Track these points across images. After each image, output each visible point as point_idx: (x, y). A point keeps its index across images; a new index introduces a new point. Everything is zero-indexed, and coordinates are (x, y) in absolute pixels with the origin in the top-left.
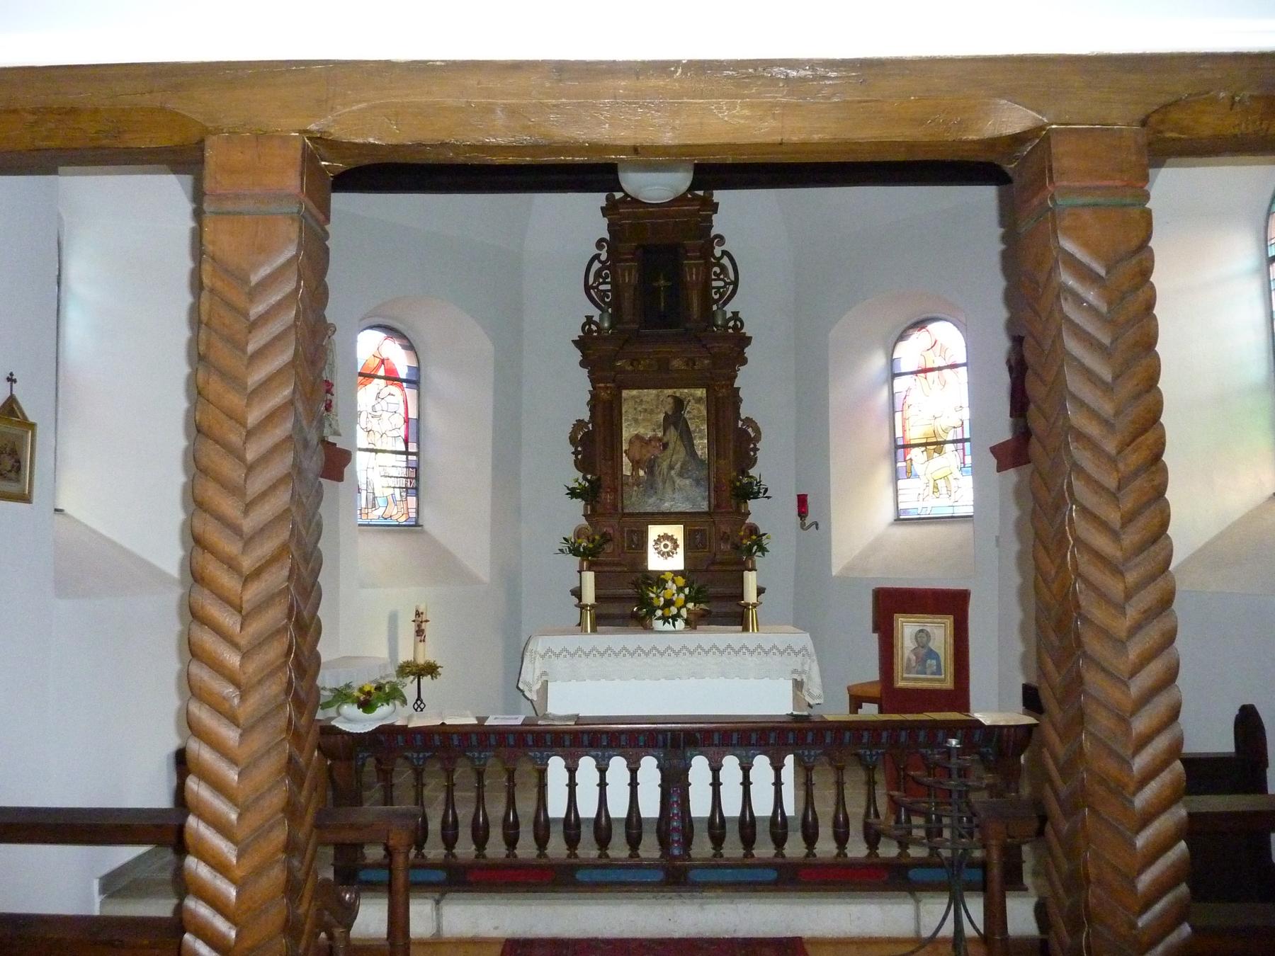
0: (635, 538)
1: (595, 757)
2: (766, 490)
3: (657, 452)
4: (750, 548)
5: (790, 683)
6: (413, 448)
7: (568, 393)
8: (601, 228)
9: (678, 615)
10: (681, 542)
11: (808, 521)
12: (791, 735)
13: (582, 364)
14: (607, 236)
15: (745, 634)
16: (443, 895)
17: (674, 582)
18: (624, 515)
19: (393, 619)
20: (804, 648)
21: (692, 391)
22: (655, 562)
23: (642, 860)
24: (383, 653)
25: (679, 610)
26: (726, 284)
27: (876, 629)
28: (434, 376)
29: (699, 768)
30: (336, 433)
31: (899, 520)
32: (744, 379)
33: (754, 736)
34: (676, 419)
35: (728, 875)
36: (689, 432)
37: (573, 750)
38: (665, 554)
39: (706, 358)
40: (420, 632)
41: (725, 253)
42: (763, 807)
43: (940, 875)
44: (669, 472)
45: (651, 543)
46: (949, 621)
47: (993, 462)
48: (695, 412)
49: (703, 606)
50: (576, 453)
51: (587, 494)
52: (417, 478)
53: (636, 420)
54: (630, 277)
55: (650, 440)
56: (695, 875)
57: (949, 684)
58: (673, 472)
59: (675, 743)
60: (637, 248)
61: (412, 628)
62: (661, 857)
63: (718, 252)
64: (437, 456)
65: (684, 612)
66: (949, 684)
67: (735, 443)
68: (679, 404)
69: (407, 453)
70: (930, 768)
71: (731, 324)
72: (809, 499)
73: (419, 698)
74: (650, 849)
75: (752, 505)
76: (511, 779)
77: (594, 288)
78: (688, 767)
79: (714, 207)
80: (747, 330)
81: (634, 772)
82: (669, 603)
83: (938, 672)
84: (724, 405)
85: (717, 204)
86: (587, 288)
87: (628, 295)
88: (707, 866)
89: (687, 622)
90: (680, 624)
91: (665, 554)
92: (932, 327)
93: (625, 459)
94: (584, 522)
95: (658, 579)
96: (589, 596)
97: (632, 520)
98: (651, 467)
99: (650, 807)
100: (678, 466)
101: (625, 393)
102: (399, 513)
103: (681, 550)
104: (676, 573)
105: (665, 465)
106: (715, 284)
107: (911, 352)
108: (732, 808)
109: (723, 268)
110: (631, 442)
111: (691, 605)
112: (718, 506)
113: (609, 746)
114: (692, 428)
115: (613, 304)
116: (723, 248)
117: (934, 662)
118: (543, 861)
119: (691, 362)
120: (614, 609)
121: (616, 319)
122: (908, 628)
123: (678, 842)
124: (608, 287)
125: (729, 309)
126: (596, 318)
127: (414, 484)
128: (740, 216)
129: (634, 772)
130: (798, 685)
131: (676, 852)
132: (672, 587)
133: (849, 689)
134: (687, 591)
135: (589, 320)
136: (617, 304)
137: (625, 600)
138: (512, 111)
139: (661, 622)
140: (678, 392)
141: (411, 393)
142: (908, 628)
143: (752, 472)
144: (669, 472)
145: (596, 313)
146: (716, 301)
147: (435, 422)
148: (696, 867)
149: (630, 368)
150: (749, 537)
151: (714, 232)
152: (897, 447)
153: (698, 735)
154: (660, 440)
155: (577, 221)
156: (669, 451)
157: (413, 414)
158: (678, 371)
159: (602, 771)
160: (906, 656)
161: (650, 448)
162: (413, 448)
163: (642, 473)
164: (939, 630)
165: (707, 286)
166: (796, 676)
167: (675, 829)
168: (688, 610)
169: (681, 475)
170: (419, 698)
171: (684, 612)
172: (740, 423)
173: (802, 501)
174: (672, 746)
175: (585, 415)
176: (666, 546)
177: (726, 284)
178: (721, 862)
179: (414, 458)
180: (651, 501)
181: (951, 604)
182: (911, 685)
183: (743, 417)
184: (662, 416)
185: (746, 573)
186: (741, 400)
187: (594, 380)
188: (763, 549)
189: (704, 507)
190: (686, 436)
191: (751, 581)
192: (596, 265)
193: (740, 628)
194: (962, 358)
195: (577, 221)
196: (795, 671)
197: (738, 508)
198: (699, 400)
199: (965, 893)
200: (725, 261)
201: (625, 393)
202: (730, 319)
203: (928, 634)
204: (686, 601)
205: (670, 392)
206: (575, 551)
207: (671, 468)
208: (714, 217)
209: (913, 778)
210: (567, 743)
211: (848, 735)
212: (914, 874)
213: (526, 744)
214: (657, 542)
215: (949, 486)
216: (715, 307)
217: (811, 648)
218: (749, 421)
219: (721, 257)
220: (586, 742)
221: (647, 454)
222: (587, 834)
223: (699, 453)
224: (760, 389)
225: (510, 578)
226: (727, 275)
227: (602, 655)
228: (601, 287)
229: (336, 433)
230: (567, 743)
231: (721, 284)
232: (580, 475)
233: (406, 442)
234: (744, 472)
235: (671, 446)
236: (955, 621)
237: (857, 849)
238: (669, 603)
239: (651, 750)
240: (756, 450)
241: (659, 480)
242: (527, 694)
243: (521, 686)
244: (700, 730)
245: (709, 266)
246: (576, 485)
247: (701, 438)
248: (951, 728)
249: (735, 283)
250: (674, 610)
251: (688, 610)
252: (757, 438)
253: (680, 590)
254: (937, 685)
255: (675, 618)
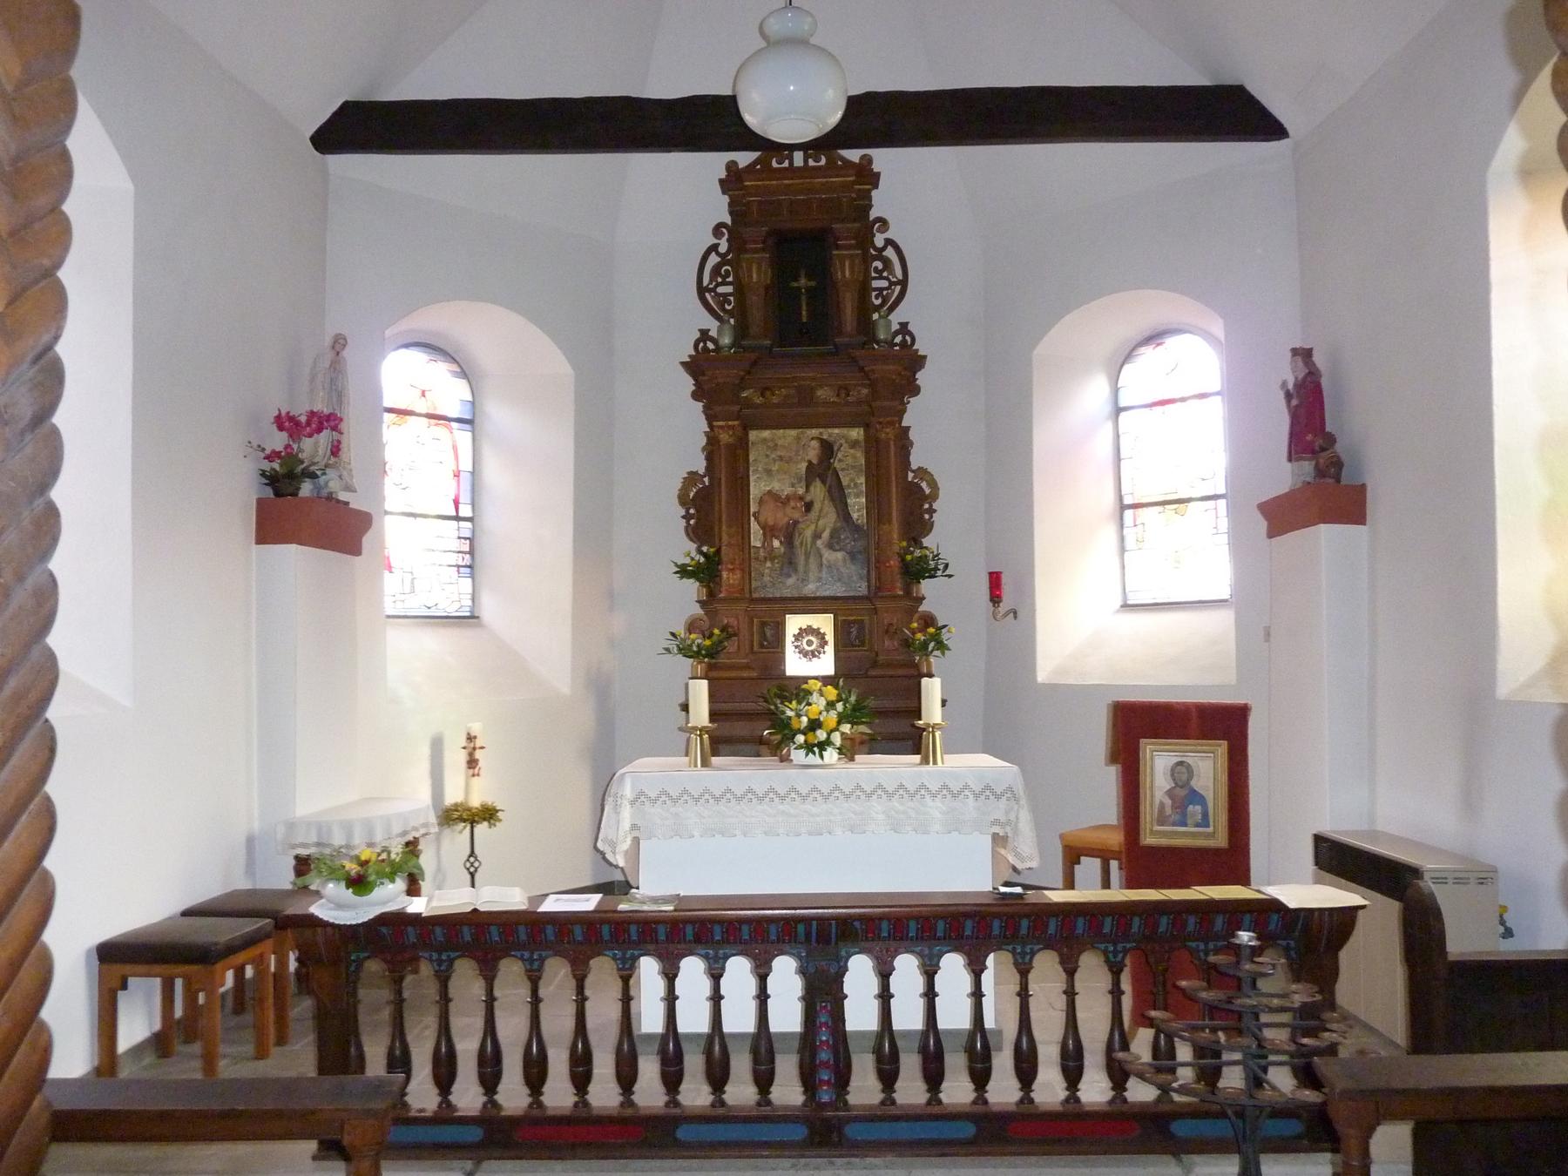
0: (769, 633)
1: (706, 957)
2: (946, 566)
3: (796, 515)
4: (925, 645)
5: (989, 838)
6: (465, 511)
7: (677, 435)
8: (719, 209)
9: (827, 743)
10: (830, 638)
11: (1004, 606)
12: (996, 924)
13: (696, 396)
14: (728, 220)
15: (925, 768)
16: (479, 1162)
17: (821, 694)
18: (753, 600)
19: (437, 745)
20: (1010, 789)
21: (844, 431)
22: (795, 665)
23: (775, 1109)
24: (421, 796)
25: (829, 735)
26: (891, 284)
27: (1114, 758)
28: (497, 413)
29: (860, 973)
30: (349, 488)
31: (1126, 606)
32: (915, 415)
33: (941, 925)
34: (823, 469)
35: (904, 1131)
36: (841, 488)
37: (671, 947)
38: (809, 654)
39: (863, 385)
40: (472, 763)
41: (889, 242)
42: (954, 1015)
43: (1221, 1129)
44: (814, 542)
45: (789, 639)
46: (1222, 747)
47: (1262, 525)
48: (850, 461)
49: (863, 728)
50: (687, 517)
51: (705, 572)
52: (471, 552)
53: (769, 472)
54: (758, 274)
55: (788, 498)
56: (853, 1131)
57: (1221, 840)
58: (819, 543)
59: (823, 936)
60: (769, 234)
61: (462, 757)
62: (805, 1105)
63: (879, 240)
64: (496, 521)
65: (837, 738)
66: (1221, 840)
67: (906, 502)
68: (828, 449)
69: (457, 518)
70: (1212, 975)
71: (898, 339)
72: (1004, 579)
73: (472, 854)
74: (788, 1091)
75: (926, 587)
76: (580, 989)
77: (710, 291)
78: (844, 970)
79: (874, 179)
80: (921, 347)
81: (762, 979)
82: (815, 725)
83: (1205, 822)
84: (889, 452)
85: (878, 174)
86: (702, 291)
87: (755, 300)
88: (870, 1117)
89: (840, 750)
90: (831, 755)
91: (809, 654)
92: (1172, 342)
93: (754, 526)
94: (697, 610)
95: (797, 690)
96: (701, 713)
97: (764, 607)
98: (790, 534)
99: (787, 1016)
100: (826, 535)
101: (753, 435)
102: (453, 595)
103: (830, 649)
104: (826, 680)
105: (809, 533)
106: (876, 284)
107: (1148, 373)
108: (909, 1016)
109: (887, 263)
110: (761, 502)
111: (846, 728)
112: (879, 589)
113: (725, 941)
114: (845, 482)
115: (739, 315)
116: (888, 235)
117: (1198, 808)
118: (629, 1112)
119: (844, 390)
120: (740, 729)
121: (741, 332)
122: (1159, 761)
123: (828, 1083)
124: (729, 289)
125: (896, 318)
126: (713, 333)
127: (472, 562)
128: (914, 188)
129: (762, 979)
130: (999, 840)
131: (825, 1098)
132: (818, 703)
133: (1062, 837)
134: (840, 706)
135: (704, 334)
136: (741, 313)
137: (752, 718)
138: (922, 828)
139: (802, 752)
140: (827, 433)
141: (464, 437)
142: (1159, 761)
143: (926, 542)
144: (814, 542)
145: (712, 325)
146: (877, 308)
147: (496, 475)
148: (857, 1119)
149: (758, 400)
150: (923, 630)
151: (873, 214)
152: (1123, 507)
153: (857, 924)
154: (801, 498)
155: (681, 197)
156: (813, 514)
157: (466, 464)
158: (826, 403)
159: (716, 976)
160: (1157, 802)
161: (788, 510)
162: (465, 511)
163: (776, 543)
164: (1206, 765)
165: (864, 289)
166: (996, 829)
167: (825, 1064)
168: (843, 734)
169: (830, 546)
170: (472, 854)
171: (837, 738)
172: (911, 475)
173: (995, 580)
174: (818, 942)
175: (700, 465)
176: (810, 643)
177: (891, 284)
178: (892, 1111)
179: (469, 525)
180: (790, 581)
181: (1224, 724)
182: (1164, 842)
183: (914, 466)
184: (804, 465)
185: (925, 681)
186: (912, 444)
187: (710, 418)
188: (941, 646)
189: (862, 589)
190: (838, 495)
191: (932, 689)
192: (714, 259)
193: (917, 758)
194: (1216, 385)
195: (681, 197)
196: (996, 822)
197: (908, 593)
198: (854, 444)
199: (1263, 1158)
200: (890, 253)
201: (753, 435)
202: (896, 333)
203: (1189, 767)
204: (839, 723)
205: (814, 432)
206: (685, 651)
207: (817, 536)
208: (874, 193)
209: (1182, 990)
210: (662, 937)
211: (1080, 922)
212: (1180, 1128)
213: (599, 940)
214: (798, 637)
215: (1198, 555)
216: (875, 316)
217: (1020, 788)
218: (922, 472)
219: (884, 248)
220: (690, 936)
221: (781, 517)
222: (694, 1063)
223: (855, 516)
224: (935, 427)
225: (600, 689)
226: (892, 272)
227: (717, 799)
228: (721, 290)
229: (349, 488)
230: (662, 937)
231: (884, 284)
232: (692, 547)
233: (456, 503)
234: (916, 541)
235: (817, 506)
236: (1156, 734)
237: (1095, 1090)
238: (815, 725)
239: (787, 947)
240: (932, 511)
241: (801, 560)
242: (609, 856)
243: (600, 845)
244: (861, 918)
245: (866, 260)
246: (687, 561)
247: (857, 496)
248: (1237, 912)
249: (904, 283)
250: (821, 735)
251: (843, 734)
252: (934, 496)
253: (831, 705)
254: (1211, 843)
255: (822, 746)
